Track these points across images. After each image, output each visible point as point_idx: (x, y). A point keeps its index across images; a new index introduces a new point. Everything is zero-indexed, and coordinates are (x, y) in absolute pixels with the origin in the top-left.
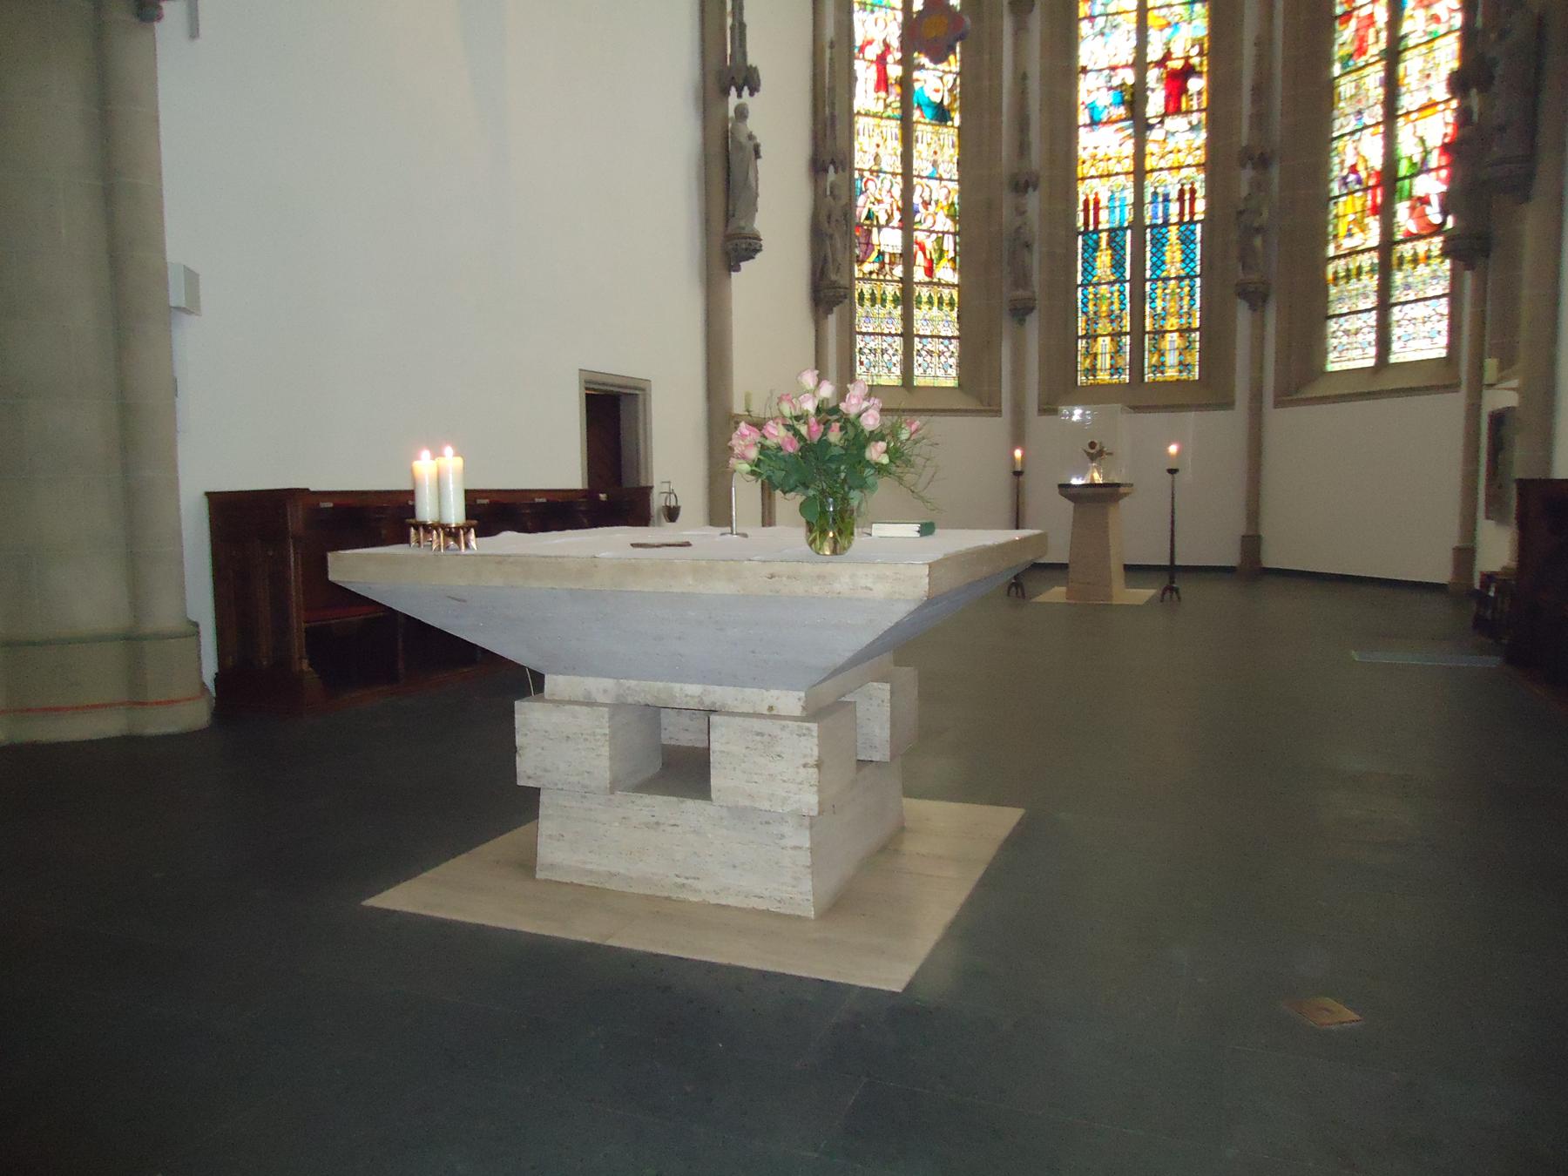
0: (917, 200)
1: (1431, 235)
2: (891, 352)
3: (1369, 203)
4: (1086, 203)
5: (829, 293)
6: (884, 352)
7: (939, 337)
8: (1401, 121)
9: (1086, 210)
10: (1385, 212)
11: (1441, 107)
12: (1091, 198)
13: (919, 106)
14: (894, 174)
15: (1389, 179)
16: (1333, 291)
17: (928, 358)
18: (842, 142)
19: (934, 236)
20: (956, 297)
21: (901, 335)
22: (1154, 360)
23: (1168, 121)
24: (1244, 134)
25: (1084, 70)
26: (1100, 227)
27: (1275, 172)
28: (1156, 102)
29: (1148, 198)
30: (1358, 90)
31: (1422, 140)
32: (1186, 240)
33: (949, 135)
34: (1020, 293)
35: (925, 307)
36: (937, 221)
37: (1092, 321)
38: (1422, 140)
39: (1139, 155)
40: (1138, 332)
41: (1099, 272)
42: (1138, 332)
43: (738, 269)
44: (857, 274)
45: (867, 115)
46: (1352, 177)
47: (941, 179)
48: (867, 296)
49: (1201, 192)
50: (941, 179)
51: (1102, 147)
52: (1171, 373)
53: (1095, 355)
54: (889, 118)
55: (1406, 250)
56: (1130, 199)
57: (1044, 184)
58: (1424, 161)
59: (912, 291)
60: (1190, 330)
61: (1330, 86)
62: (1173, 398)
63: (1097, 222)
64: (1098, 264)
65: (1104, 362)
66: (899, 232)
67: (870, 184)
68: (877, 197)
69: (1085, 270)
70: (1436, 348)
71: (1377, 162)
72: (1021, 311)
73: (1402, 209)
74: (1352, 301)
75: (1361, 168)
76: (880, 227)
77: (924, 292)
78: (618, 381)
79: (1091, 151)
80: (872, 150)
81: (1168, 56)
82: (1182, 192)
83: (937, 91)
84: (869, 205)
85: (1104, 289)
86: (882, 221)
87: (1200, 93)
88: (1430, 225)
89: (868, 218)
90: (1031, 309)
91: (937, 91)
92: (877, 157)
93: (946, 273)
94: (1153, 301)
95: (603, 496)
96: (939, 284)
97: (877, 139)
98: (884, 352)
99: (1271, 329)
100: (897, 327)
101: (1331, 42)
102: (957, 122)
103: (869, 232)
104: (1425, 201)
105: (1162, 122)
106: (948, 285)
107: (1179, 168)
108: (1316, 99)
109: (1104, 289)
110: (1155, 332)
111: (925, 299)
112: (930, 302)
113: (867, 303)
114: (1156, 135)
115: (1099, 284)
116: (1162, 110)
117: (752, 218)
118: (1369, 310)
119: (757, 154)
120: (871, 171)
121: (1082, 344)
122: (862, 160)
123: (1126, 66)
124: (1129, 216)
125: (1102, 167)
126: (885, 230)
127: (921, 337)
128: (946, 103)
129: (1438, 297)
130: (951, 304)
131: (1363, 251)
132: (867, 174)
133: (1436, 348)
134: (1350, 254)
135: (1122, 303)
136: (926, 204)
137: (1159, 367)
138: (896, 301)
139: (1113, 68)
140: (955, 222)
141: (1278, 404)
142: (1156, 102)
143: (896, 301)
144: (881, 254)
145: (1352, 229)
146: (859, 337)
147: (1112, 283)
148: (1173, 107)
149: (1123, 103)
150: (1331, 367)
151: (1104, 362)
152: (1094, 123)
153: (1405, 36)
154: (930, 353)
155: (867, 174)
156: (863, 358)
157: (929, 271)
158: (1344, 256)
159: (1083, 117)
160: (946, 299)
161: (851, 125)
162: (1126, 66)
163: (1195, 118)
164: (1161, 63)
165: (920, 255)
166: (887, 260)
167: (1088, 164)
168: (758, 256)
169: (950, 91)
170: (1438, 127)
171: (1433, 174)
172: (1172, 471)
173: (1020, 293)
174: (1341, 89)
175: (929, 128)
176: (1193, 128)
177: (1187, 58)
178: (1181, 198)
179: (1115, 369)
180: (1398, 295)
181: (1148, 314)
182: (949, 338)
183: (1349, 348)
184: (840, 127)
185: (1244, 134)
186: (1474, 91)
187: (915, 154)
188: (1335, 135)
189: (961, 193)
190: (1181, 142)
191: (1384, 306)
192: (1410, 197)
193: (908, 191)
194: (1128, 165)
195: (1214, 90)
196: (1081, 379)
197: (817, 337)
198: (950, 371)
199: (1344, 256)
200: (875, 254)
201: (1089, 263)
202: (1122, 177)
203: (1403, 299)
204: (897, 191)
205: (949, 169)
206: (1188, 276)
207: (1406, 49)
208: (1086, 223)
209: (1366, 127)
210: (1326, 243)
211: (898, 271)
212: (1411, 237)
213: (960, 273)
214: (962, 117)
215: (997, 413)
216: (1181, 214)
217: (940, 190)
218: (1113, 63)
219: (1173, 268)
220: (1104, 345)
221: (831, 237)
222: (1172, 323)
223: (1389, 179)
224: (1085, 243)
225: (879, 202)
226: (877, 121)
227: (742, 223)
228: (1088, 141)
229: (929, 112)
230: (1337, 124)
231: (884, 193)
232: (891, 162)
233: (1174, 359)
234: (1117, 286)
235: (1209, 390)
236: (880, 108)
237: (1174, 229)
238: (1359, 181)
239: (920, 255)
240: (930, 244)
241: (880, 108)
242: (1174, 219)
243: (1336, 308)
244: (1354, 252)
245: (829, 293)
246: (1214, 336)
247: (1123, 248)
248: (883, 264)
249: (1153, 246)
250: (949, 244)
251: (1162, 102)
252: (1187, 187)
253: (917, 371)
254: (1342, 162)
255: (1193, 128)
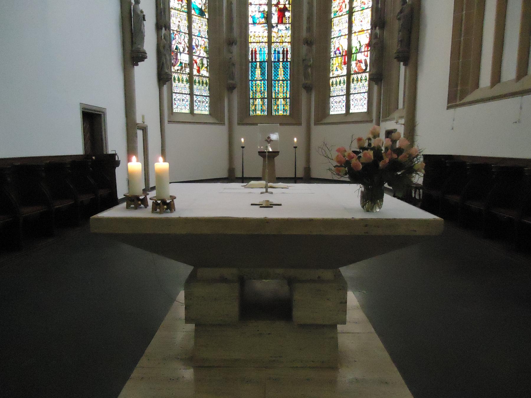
0: (194, 44)
1: (362, 73)
2: (186, 100)
3: (343, 61)
4: (252, 51)
5: (164, 78)
6: (183, 100)
7: (202, 96)
8: (353, 35)
9: (252, 54)
10: (348, 64)
11: (365, 32)
12: (254, 49)
13: (194, 9)
14: (185, 33)
15: (349, 53)
16: (332, 88)
17: (199, 103)
18: (167, 19)
19: (200, 58)
20: (208, 81)
21: (189, 94)
22: (253, 108)
23: (279, 25)
24: (304, 34)
25: (251, 4)
26: (257, 60)
27: (314, 47)
28: (275, 19)
29: (273, 52)
30: (339, 26)
31: (359, 42)
32: (284, 67)
33: (204, 21)
34: (231, 82)
35: (197, 84)
36: (201, 52)
37: (255, 93)
38: (359, 42)
39: (270, 37)
40: (270, 98)
41: (256, 76)
42: (270, 98)
43: (137, 65)
44: (173, 70)
45: (175, 9)
46: (338, 52)
47: (202, 37)
48: (177, 79)
49: (289, 52)
50: (202, 37)
51: (257, 32)
52: (281, 113)
53: (256, 105)
54: (183, 11)
55: (355, 76)
56: (267, 52)
57: (238, 43)
58: (360, 49)
59: (193, 78)
60: (286, 98)
61: (331, 21)
62: (283, 121)
63: (256, 58)
64: (256, 73)
65: (259, 107)
66: (188, 56)
67: (177, 36)
68: (179, 42)
69: (252, 75)
70: (364, 109)
71: (346, 48)
72: (231, 88)
73: (353, 63)
74: (337, 90)
75: (340, 49)
76: (180, 53)
77: (196, 79)
78: (94, 108)
79: (253, 33)
80: (177, 23)
81: (278, 3)
82: (283, 51)
83: (200, 4)
84: (176, 44)
85: (258, 82)
86: (181, 51)
87: (289, 17)
88: (362, 70)
89: (176, 49)
90: (235, 88)
91: (200, 4)
92: (179, 26)
93: (204, 72)
94: (275, 87)
95: (94, 158)
96: (202, 76)
97: (179, 19)
98: (183, 100)
99: (313, 99)
100: (187, 91)
101: (331, 6)
102: (207, 17)
103: (177, 54)
104: (360, 62)
105: (277, 26)
106: (205, 77)
107: (283, 42)
108: (326, 24)
109: (258, 82)
110: (276, 98)
111: (197, 82)
112: (199, 82)
113: (177, 82)
114: (275, 30)
115: (257, 80)
116: (277, 22)
117: (143, 46)
118: (343, 95)
119: (144, 20)
120: (177, 31)
121: (251, 101)
122: (173, 27)
123: (265, 4)
124: (266, 58)
125: (257, 40)
126: (182, 54)
127: (197, 95)
128: (203, 9)
129: (364, 93)
130: (206, 84)
131: (341, 76)
132: (175, 32)
133: (364, 109)
134: (337, 77)
135: (264, 88)
136: (197, 46)
137: (277, 110)
138: (187, 81)
139: (260, 5)
140: (207, 54)
141: (315, 124)
142: (275, 19)
143: (187, 81)
144: (181, 63)
145: (337, 69)
146: (195, 96)
147: (261, 80)
148: (281, 21)
149: (264, 17)
150: (331, 113)
151: (259, 107)
152: (254, 23)
153: (354, 8)
154: (199, 101)
155: (175, 32)
156: (176, 102)
157: (199, 71)
158: (335, 77)
159: (250, 21)
160: (205, 82)
161: (169, 12)
162: (265, 4)
163: (288, 26)
164: (277, 5)
165: (195, 65)
166: (183, 66)
167: (253, 37)
168: (146, 60)
169: (204, 5)
170: (365, 39)
171: (363, 53)
172: (295, 147)
173: (231, 82)
174: (334, 22)
175: (197, 17)
176: (287, 29)
177: (285, 5)
178: (283, 53)
179: (262, 110)
180: (352, 91)
181: (270, 93)
182: (206, 96)
183: (337, 108)
184: (167, 13)
185: (304, 34)
186: (377, 28)
187: (193, 27)
188: (332, 37)
189: (209, 43)
190: (283, 33)
191: (348, 94)
192: (356, 60)
193: (190, 40)
194: (266, 40)
195: (294, 16)
196: (251, 113)
197: (160, 93)
198: (187, 107)
199: (335, 77)
200: (179, 63)
201: (253, 72)
202: (264, 44)
203: (354, 92)
204: (186, 40)
205: (205, 34)
206: (286, 80)
207: (354, 12)
208: (252, 59)
209: (342, 36)
210: (330, 72)
211: (188, 70)
212: (356, 73)
213: (209, 73)
214: (209, 15)
215: (224, 124)
216: (283, 58)
217: (201, 42)
218: (261, 3)
219: (281, 77)
220: (258, 102)
221: (165, 55)
222: (281, 95)
223: (349, 53)
224: (252, 66)
225: (180, 43)
226: (179, 12)
227: (139, 46)
228: (252, 29)
229: (197, 11)
230: (333, 33)
231: (182, 40)
232: (184, 28)
233: (282, 108)
234: (263, 82)
235: (293, 118)
236: (179, 7)
237: (281, 63)
238: (340, 53)
239: (195, 65)
240: (198, 61)
241: (179, 7)
242: (281, 60)
243: (332, 94)
244: (338, 76)
245: (164, 78)
246: (294, 101)
247: (265, 68)
248: (182, 67)
249: (275, 68)
250: (205, 61)
251: (277, 20)
252: (285, 49)
253: (195, 108)
254: (334, 47)
255: (287, 29)
